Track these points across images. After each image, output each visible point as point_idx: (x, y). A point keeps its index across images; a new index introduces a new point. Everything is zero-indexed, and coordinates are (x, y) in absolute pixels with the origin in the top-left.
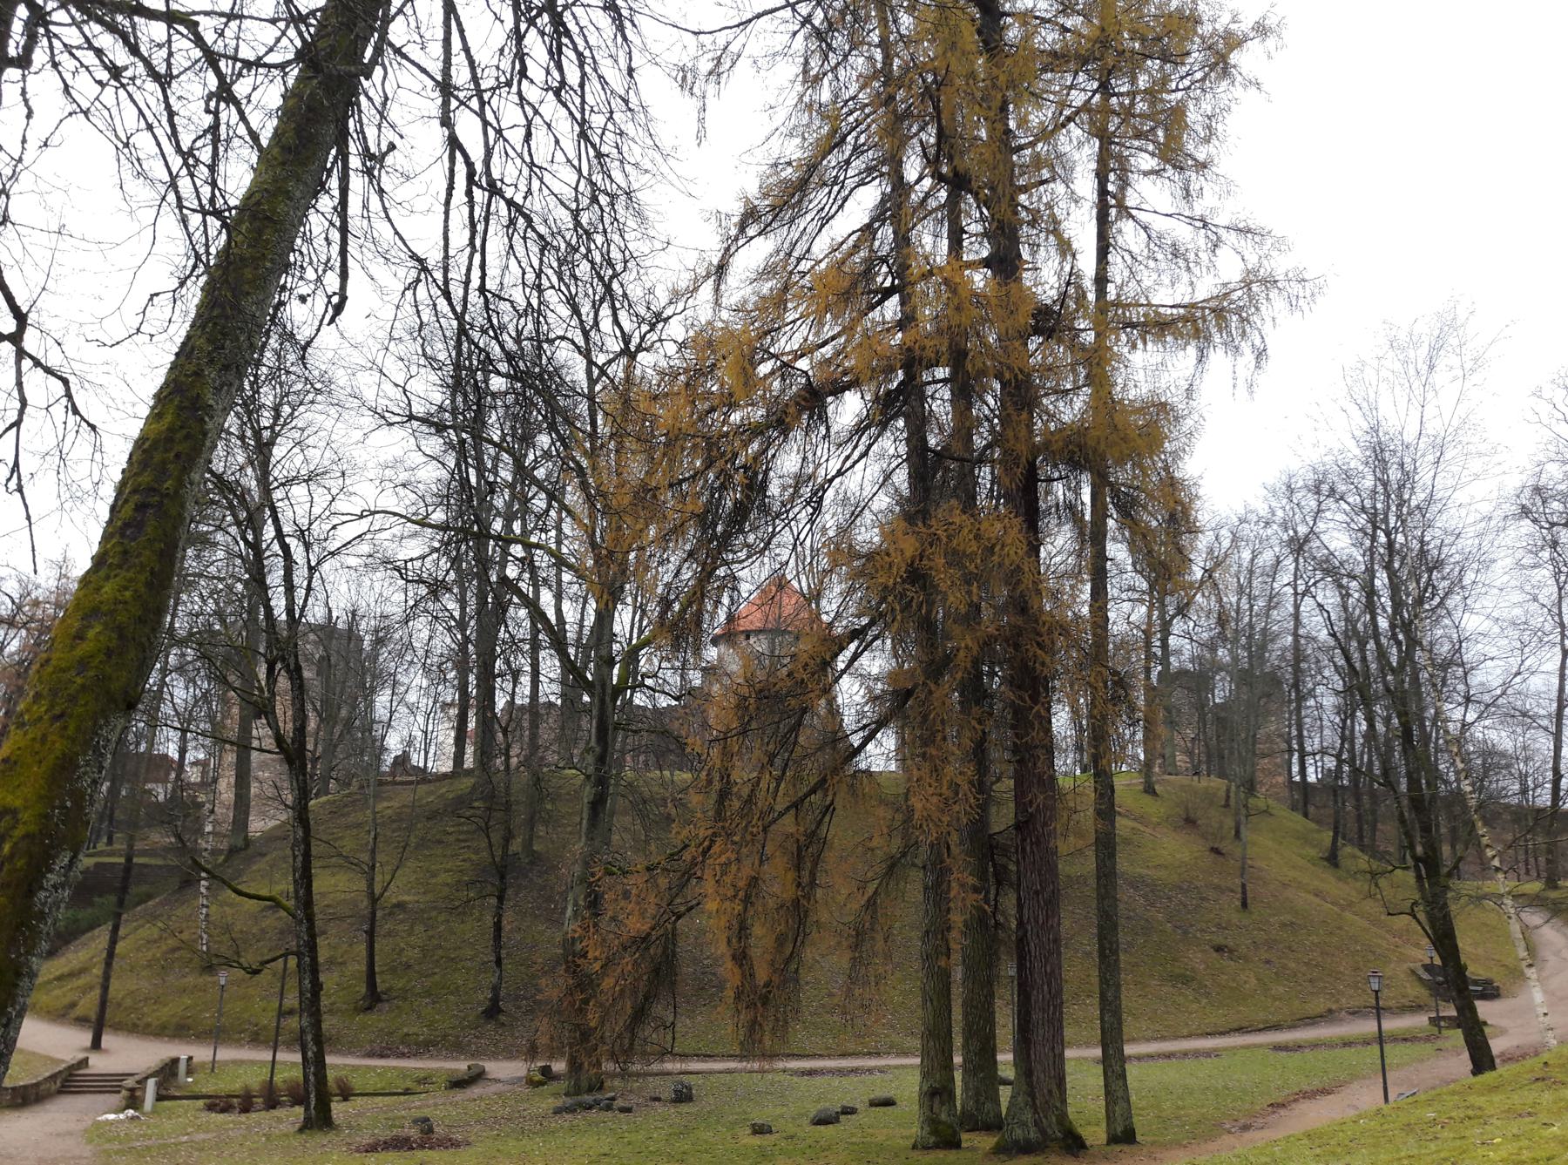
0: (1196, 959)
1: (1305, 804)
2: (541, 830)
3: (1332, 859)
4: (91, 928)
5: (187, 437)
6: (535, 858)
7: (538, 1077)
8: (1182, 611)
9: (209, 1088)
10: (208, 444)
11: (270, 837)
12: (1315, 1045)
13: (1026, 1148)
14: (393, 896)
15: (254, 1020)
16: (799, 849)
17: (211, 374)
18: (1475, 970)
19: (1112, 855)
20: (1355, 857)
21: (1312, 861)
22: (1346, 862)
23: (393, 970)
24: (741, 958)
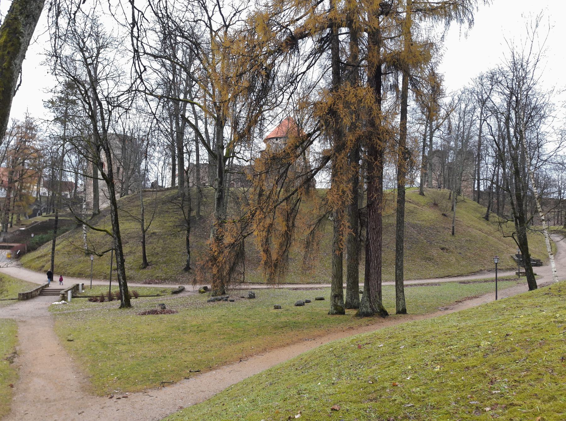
0: (434, 252)
1: (478, 199)
2: (202, 208)
3: (487, 218)
4: (48, 241)
5: (12, 45)
6: (201, 217)
7: (203, 290)
8: (438, 128)
9: (90, 293)
10: (22, 48)
11: (106, 210)
12: (474, 282)
13: (367, 315)
14: (151, 230)
15: (104, 272)
16: (288, 215)
17: (21, 18)
18: (533, 256)
19: (403, 216)
20: (494, 217)
21: (479, 218)
22: (491, 219)
23: (152, 255)
24: (267, 251)
